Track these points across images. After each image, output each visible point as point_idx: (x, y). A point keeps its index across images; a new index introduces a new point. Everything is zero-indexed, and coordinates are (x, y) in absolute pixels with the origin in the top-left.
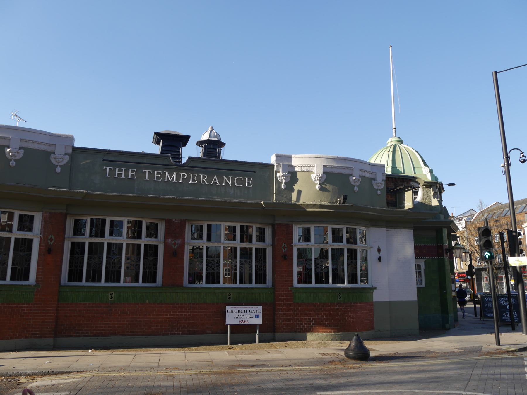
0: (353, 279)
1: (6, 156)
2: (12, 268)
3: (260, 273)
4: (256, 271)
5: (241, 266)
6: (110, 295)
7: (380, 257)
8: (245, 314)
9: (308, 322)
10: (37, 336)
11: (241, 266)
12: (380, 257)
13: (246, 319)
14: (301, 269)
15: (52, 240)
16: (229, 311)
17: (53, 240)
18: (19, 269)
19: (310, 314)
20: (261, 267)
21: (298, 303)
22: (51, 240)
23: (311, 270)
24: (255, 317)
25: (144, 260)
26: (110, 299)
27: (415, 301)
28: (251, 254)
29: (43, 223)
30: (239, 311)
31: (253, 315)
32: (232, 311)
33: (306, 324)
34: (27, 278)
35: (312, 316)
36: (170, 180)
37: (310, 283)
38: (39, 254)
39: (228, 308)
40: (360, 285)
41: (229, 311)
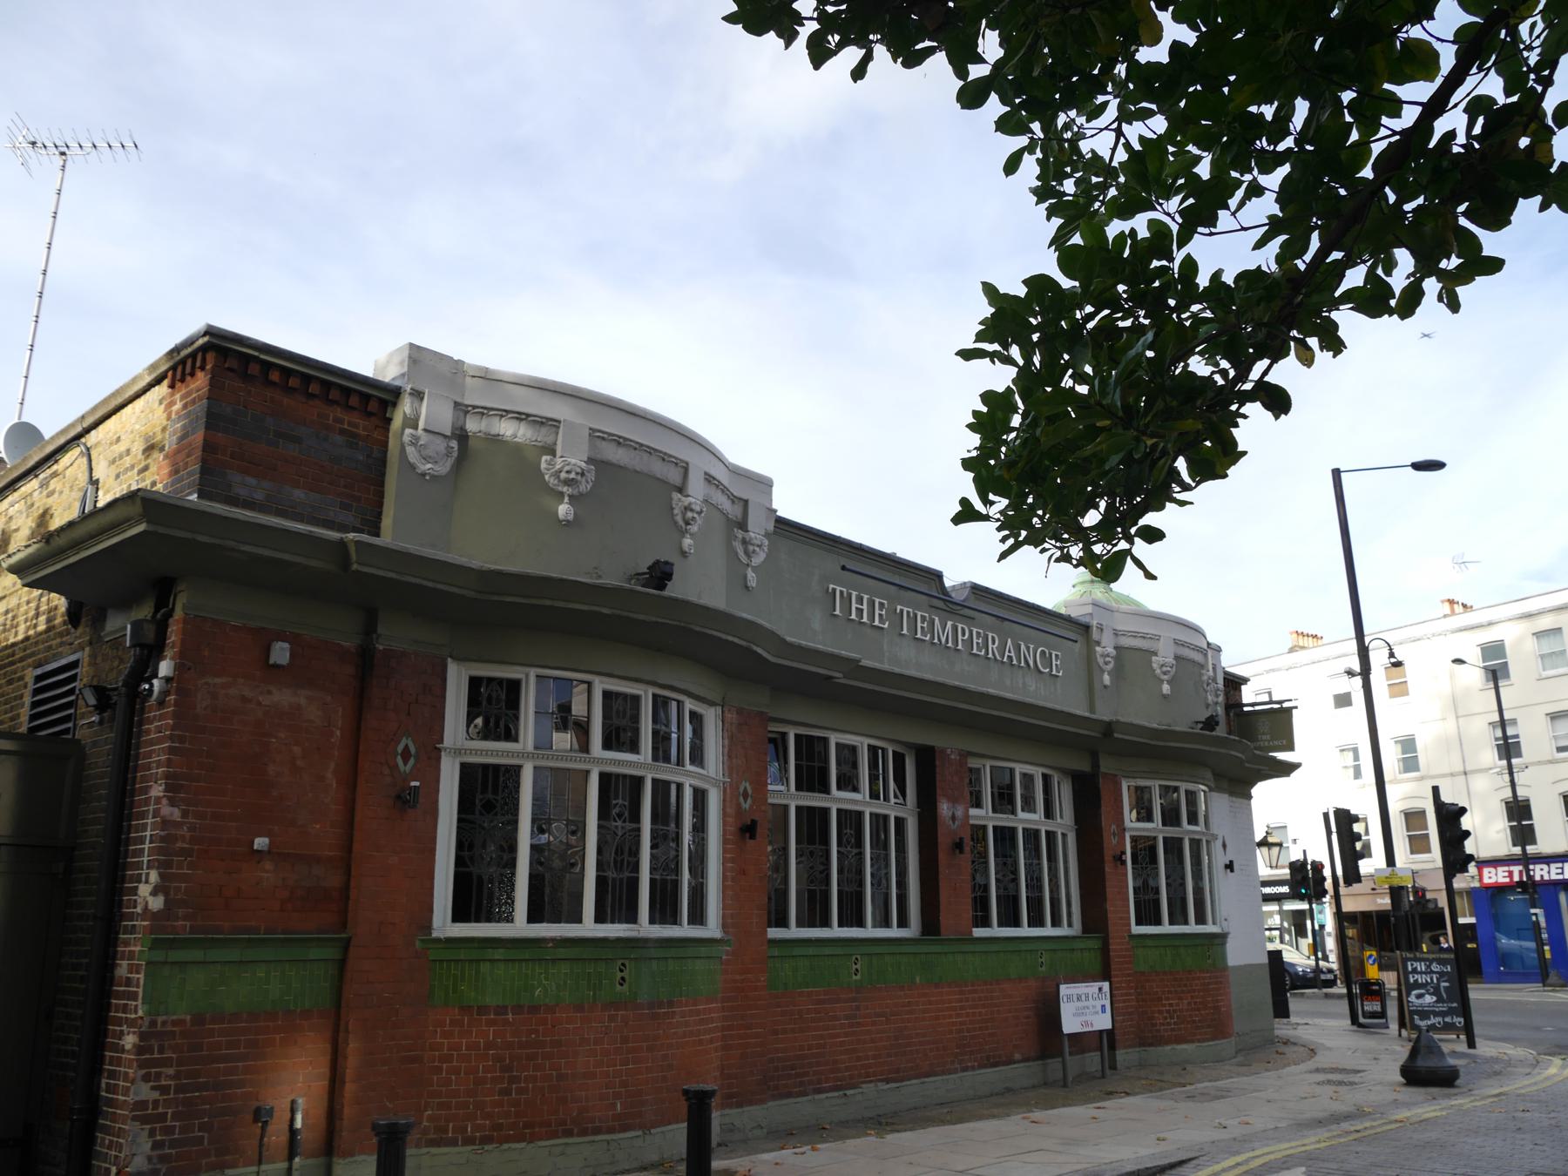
0: (1201, 920)
1: (1151, 666)
2: (839, 891)
3: (1144, 900)
4: (598, 870)
5: (1013, 877)
6: (627, 977)
7: (1231, 862)
8: (1086, 1004)
9: (1166, 1018)
10: (734, 1100)
11: (1013, 877)
12: (1231, 862)
13: (1089, 1018)
14: (1140, 883)
15: (411, 755)
16: (1065, 999)
17: (400, 752)
18: (614, 879)
19: (1168, 999)
20: (622, 854)
21: (1143, 973)
22: (406, 755)
23: (1157, 891)
24: (1100, 1012)
25: (458, 828)
26: (854, 977)
27: (1260, 966)
28: (985, 838)
29: (726, 742)
30: (1079, 998)
31: (1098, 1004)
32: (1069, 998)
33: (1163, 1024)
34: (1138, 923)
35: (1171, 1005)
36: (943, 640)
37: (577, 918)
38: (725, 841)
39: (1065, 990)
40: (1192, 928)
41: (1065, 999)
